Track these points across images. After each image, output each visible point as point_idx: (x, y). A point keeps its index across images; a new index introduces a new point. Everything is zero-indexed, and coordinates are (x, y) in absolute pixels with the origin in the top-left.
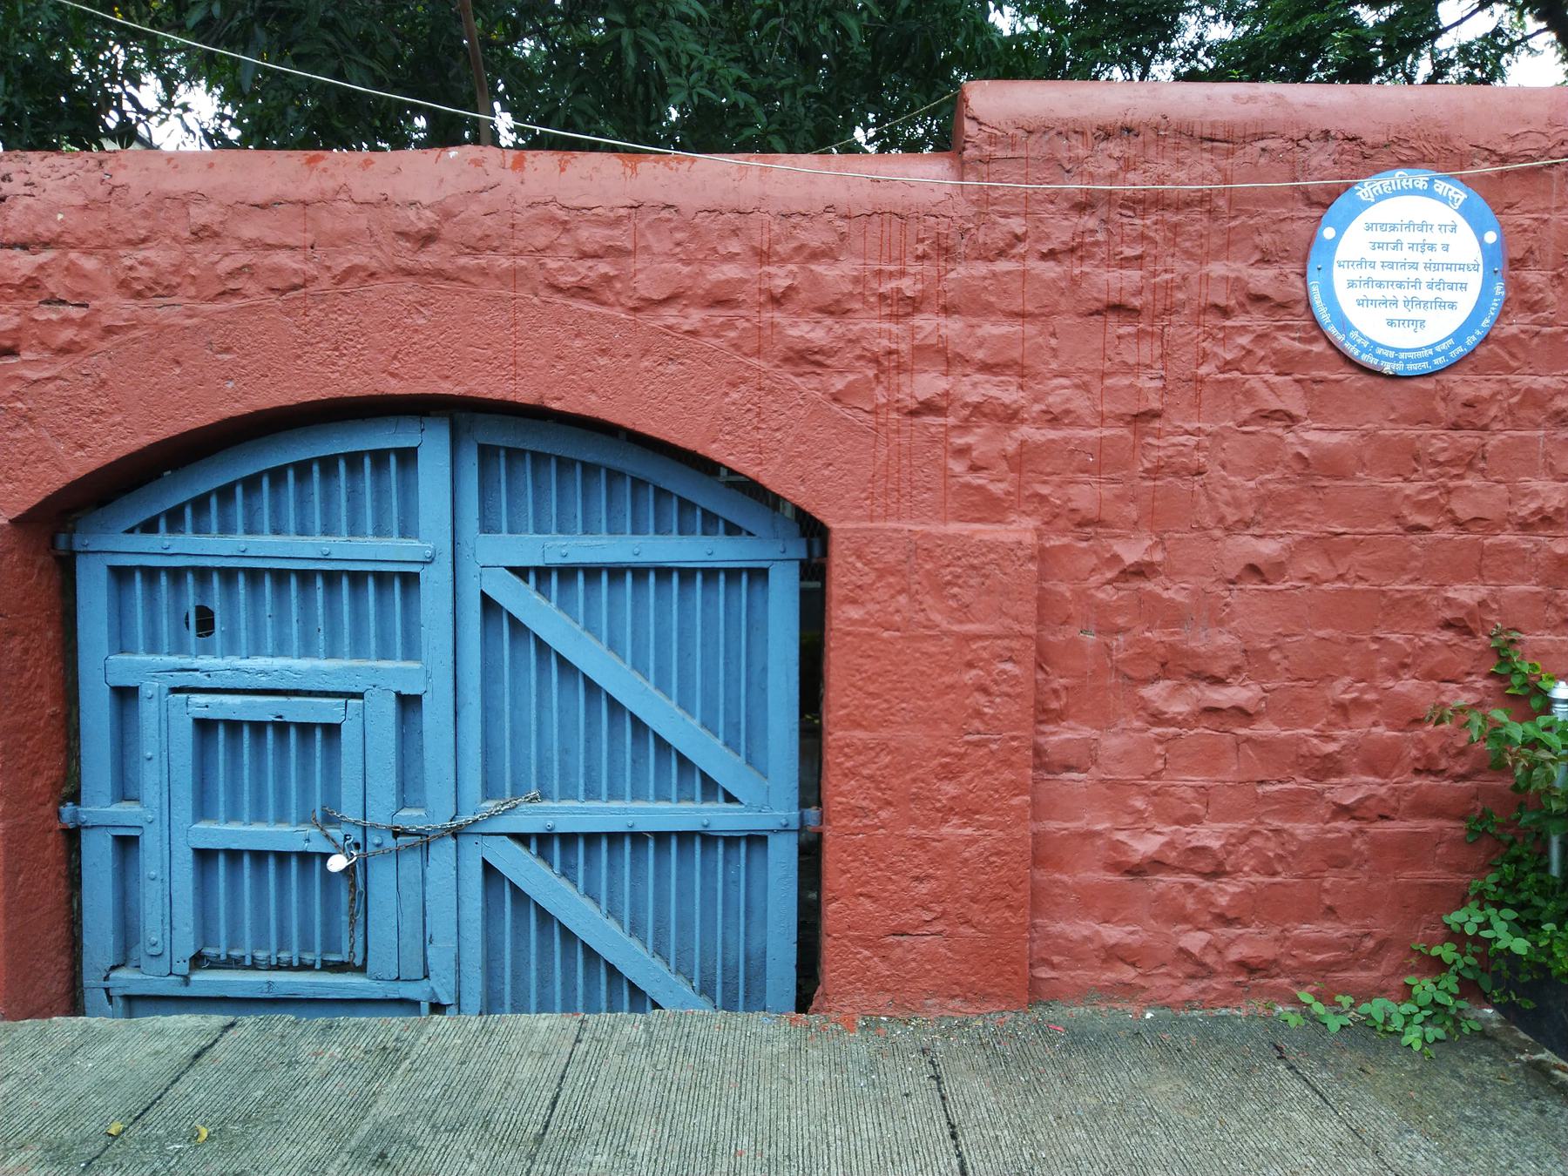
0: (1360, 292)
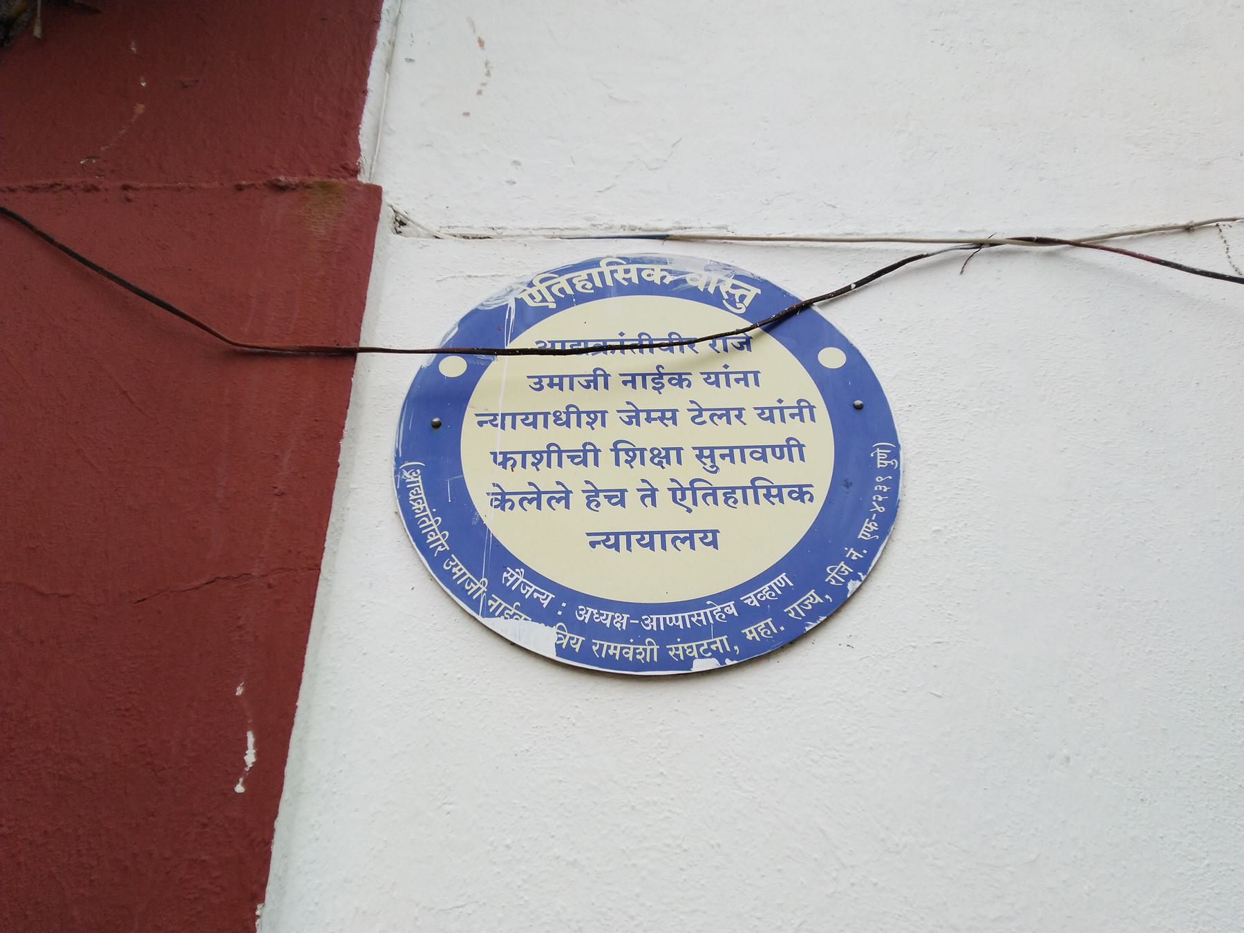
0: (516, 480)
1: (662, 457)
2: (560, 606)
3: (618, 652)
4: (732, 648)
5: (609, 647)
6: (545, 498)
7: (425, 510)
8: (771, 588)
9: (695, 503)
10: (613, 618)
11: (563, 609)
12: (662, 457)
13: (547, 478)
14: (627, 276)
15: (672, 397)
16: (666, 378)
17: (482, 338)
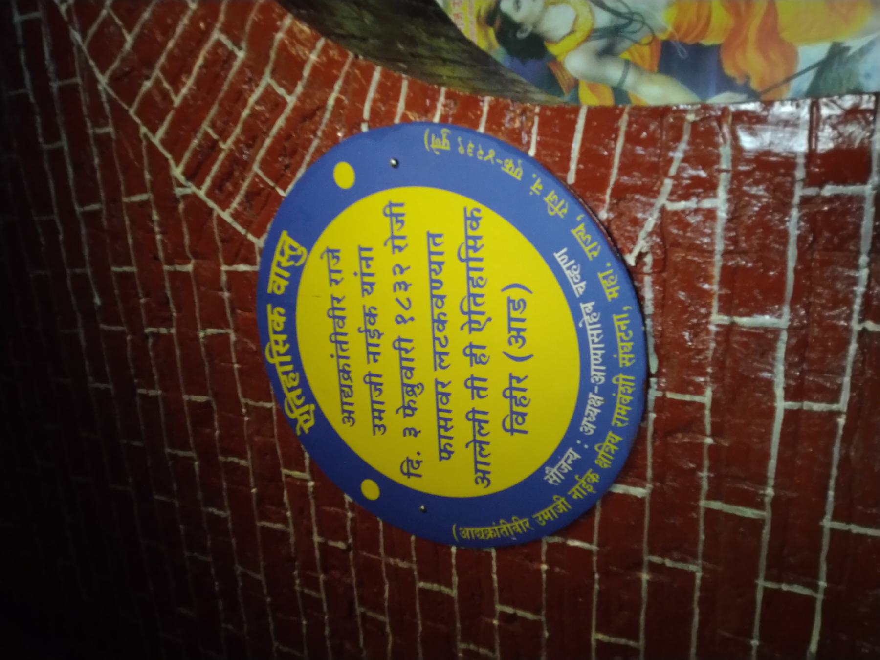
3: (624, 408)
4: (625, 312)
5: (619, 414)
6: (479, 438)
7: (494, 530)
8: (569, 268)
9: (482, 313)
10: (592, 406)
11: (582, 445)
14: (281, 343)
16: (369, 327)
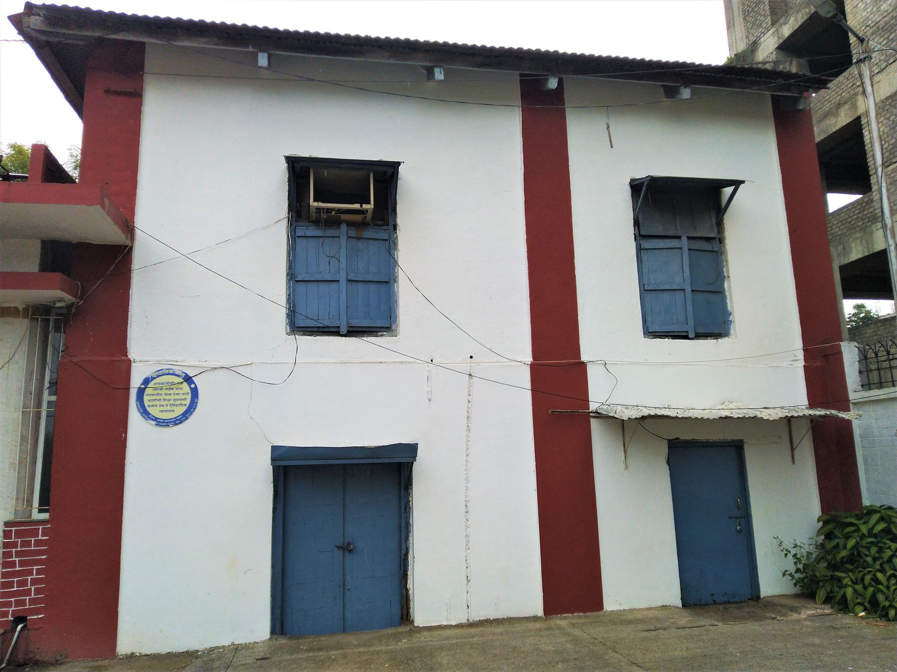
1: (169, 400)
2: (155, 419)
12: (169, 400)
13: (154, 403)
15: (171, 392)
17: (147, 381)
